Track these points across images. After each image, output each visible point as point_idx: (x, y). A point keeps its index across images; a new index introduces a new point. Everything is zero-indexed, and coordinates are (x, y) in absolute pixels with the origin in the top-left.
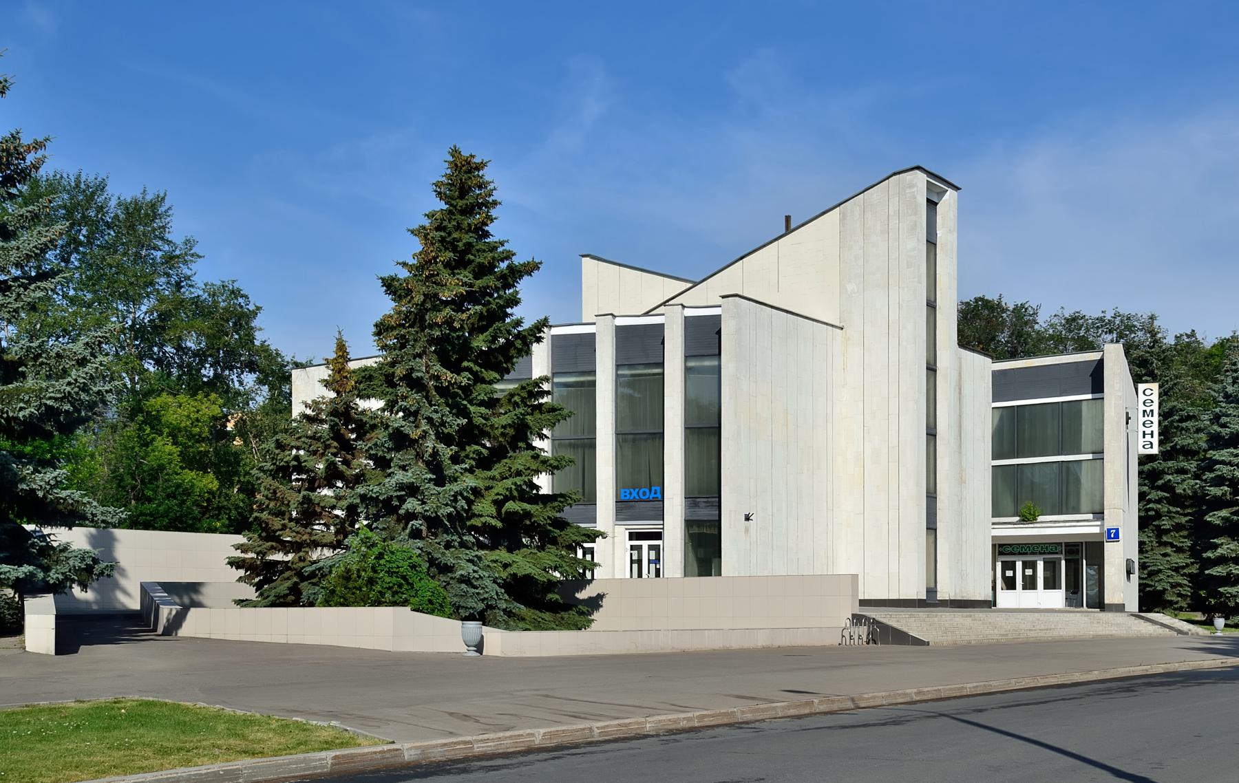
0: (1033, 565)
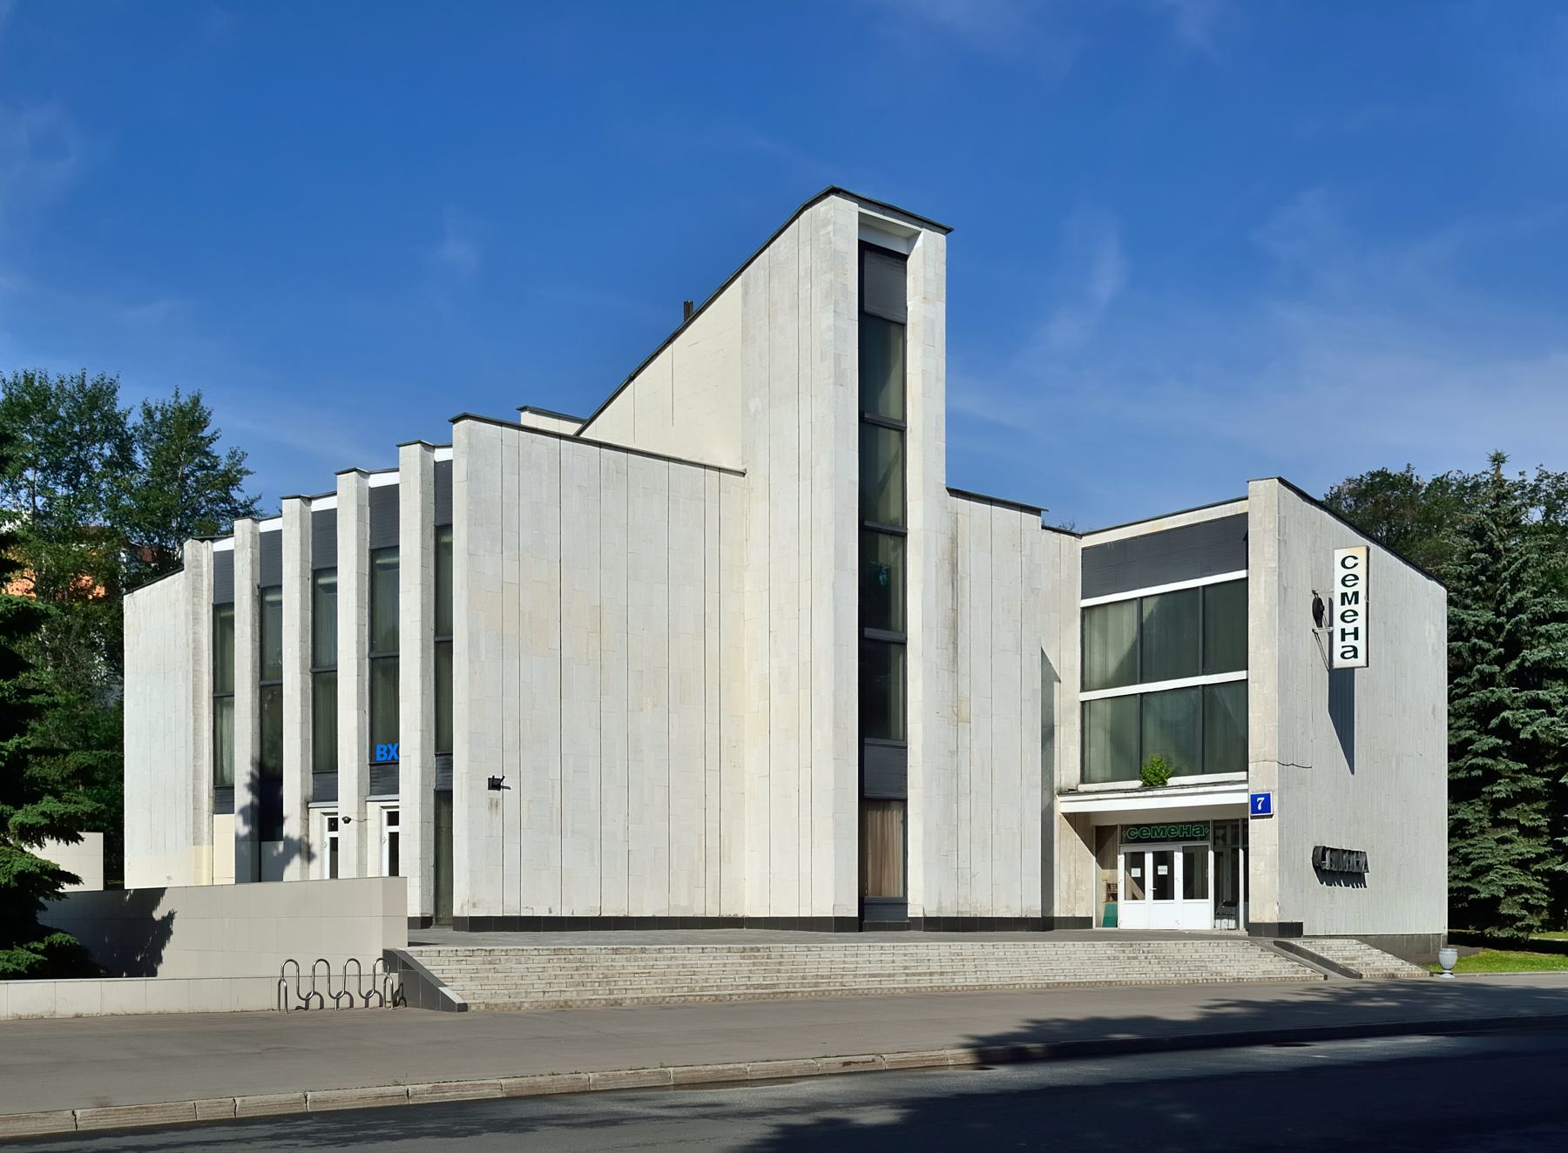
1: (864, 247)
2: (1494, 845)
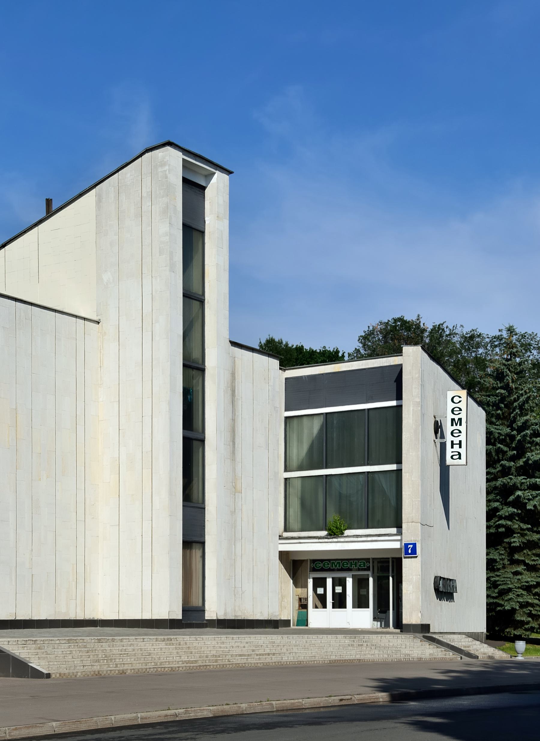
0: (342, 582)
1: (185, 181)
2: (511, 576)
